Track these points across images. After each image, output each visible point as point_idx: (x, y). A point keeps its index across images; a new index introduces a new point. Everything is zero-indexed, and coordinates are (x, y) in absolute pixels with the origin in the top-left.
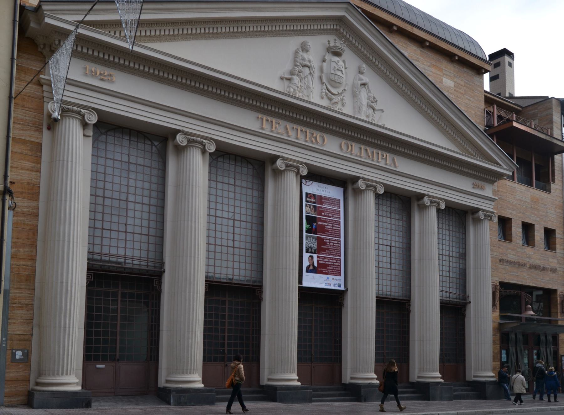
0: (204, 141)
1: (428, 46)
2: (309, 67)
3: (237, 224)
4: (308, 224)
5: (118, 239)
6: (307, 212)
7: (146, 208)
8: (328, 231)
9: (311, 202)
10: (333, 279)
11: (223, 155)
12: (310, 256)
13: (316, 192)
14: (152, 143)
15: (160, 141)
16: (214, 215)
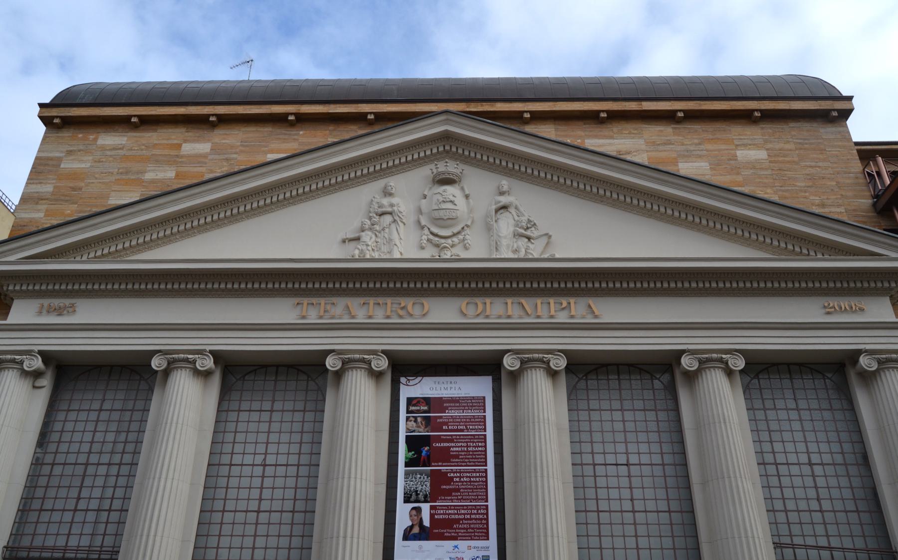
0: (724, 356)
1: (761, 117)
2: (390, 213)
3: (634, 470)
4: (409, 450)
5: (269, 524)
6: (408, 430)
7: (841, 470)
8: (457, 457)
9: (418, 412)
10: (469, 548)
11: (596, 369)
12: (413, 508)
13: (430, 392)
14: (824, 375)
15: (660, 373)
16: (773, 461)
